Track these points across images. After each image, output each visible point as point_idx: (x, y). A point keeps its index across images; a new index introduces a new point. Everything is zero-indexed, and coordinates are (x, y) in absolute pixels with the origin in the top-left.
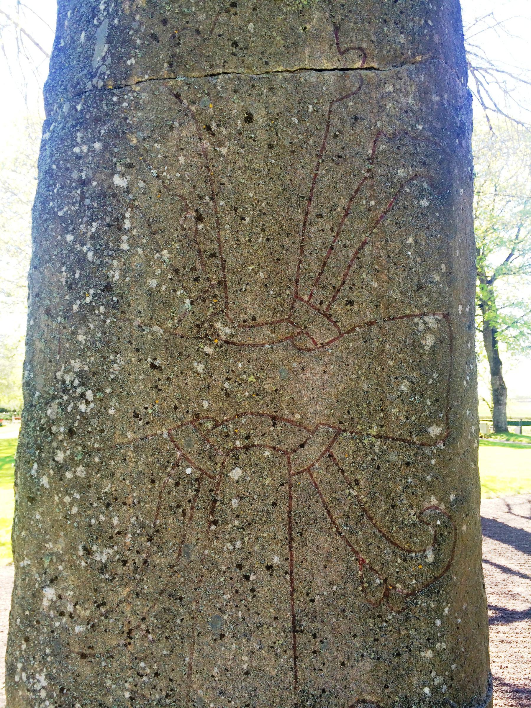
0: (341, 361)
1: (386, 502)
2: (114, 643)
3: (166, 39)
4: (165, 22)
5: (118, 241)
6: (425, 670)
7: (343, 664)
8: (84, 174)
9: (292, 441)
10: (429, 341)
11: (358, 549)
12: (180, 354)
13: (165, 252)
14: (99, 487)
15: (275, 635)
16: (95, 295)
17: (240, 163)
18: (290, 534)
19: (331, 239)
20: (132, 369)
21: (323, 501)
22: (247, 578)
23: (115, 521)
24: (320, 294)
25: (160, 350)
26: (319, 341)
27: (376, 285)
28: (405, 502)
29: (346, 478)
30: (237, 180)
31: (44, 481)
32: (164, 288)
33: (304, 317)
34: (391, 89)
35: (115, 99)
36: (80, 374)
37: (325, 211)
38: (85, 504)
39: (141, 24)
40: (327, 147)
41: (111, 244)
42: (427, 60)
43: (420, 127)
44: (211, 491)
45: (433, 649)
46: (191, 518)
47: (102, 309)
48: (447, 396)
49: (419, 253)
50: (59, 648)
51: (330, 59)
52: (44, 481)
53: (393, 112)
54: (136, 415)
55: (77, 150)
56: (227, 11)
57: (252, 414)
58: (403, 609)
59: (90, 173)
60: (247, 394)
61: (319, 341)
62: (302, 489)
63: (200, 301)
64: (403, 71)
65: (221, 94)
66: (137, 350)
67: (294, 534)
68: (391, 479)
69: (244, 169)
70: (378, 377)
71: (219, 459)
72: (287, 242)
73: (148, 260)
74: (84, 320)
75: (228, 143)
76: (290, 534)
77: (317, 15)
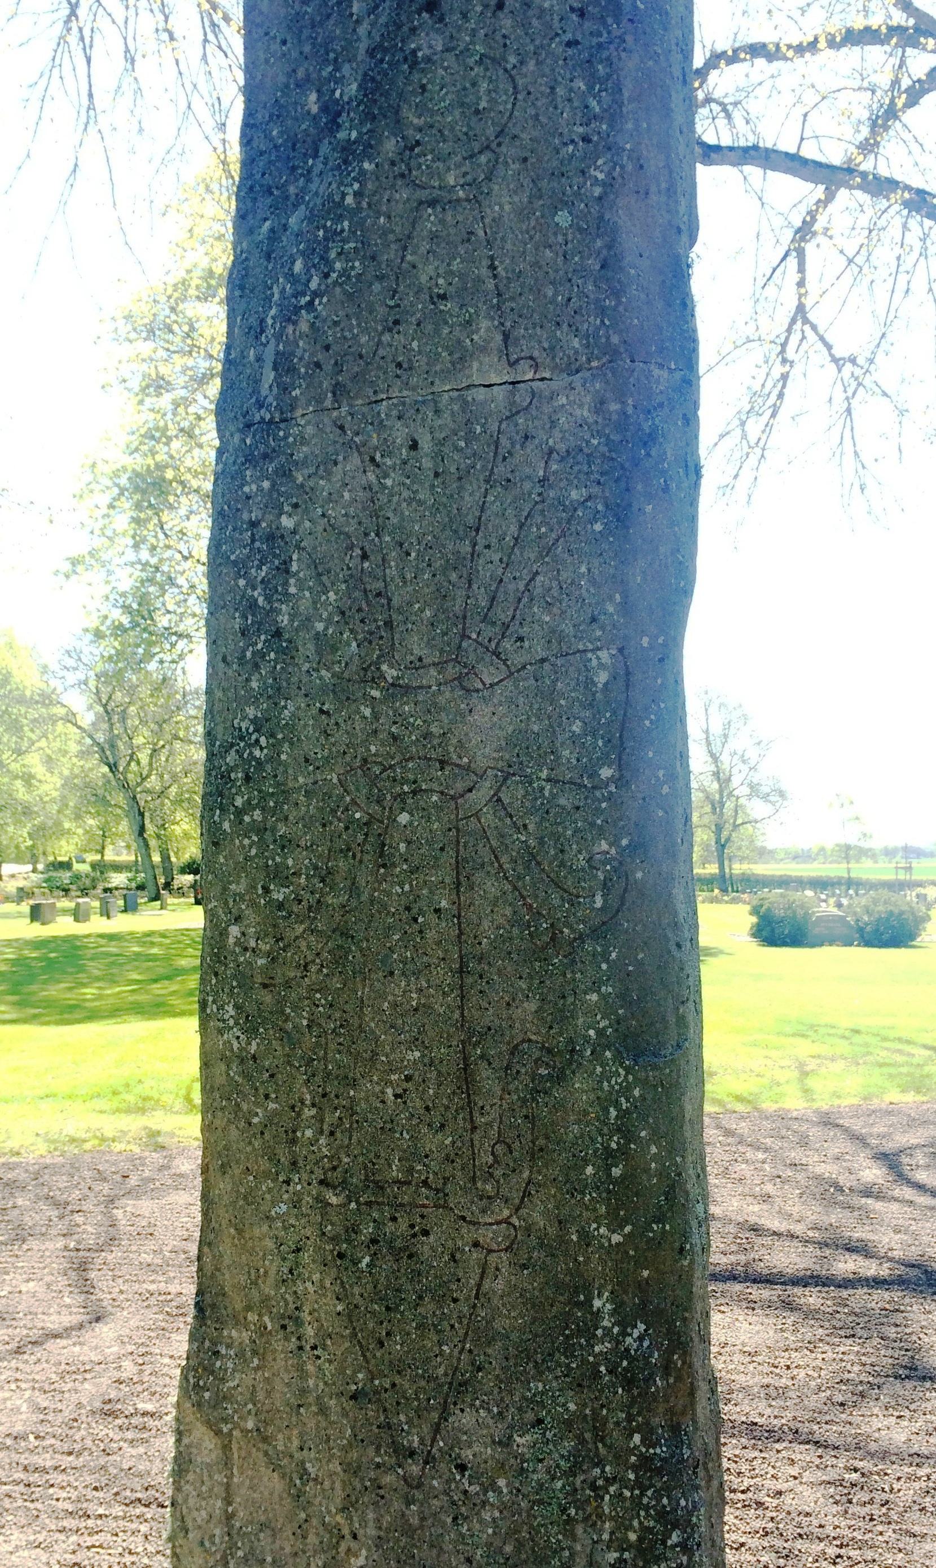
0: (511, 701)
1: (555, 848)
2: (292, 974)
3: (328, 367)
5: (286, 584)
6: (591, 1013)
8: (253, 515)
9: (460, 786)
10: (602, 677)
11: (525, 893)
12: (348, 698)
13: (331, 594)
14: (274, 830)
15: (443, 975)
16: (265, 641)
17: (406, 494)
19: (500, 571)
22: (415, 920)
24: (489, 631)
25: (328, 695)
26: (488, 682)
29: (515, 823)
30: (402, 513)
31: (226, 826)
32: (330, 631)
33: (472, 657)
34: (564, 400)
35: (281, 433)
36: (254, 721)
37: (494, 541)
38: (262, 845)
40: (496, 470)
42: (604, 365)
43: (595, 442)
44: (380, 835)
45: (599, 992)
47: (272, 655)
49: (593, 582)
50: (244, 980)
51: (499, 373)
52: (226, 826)
53: (566, 427)
54: (307, 760)
55: (246, 489)
56: (390, 330)
58: (570, 954)
59: (260, 514)
61: (488, 682)
62: (470, 834)
63: (366, 644)
65: (385, 423)
66: (306, 695)
67: (462, 879)
69: (410, 501)
70: (549, 717)
71: (387, 803)
73: (315, 603)
74: (257, 666)
76: (458, 878)
77: (484, 324)
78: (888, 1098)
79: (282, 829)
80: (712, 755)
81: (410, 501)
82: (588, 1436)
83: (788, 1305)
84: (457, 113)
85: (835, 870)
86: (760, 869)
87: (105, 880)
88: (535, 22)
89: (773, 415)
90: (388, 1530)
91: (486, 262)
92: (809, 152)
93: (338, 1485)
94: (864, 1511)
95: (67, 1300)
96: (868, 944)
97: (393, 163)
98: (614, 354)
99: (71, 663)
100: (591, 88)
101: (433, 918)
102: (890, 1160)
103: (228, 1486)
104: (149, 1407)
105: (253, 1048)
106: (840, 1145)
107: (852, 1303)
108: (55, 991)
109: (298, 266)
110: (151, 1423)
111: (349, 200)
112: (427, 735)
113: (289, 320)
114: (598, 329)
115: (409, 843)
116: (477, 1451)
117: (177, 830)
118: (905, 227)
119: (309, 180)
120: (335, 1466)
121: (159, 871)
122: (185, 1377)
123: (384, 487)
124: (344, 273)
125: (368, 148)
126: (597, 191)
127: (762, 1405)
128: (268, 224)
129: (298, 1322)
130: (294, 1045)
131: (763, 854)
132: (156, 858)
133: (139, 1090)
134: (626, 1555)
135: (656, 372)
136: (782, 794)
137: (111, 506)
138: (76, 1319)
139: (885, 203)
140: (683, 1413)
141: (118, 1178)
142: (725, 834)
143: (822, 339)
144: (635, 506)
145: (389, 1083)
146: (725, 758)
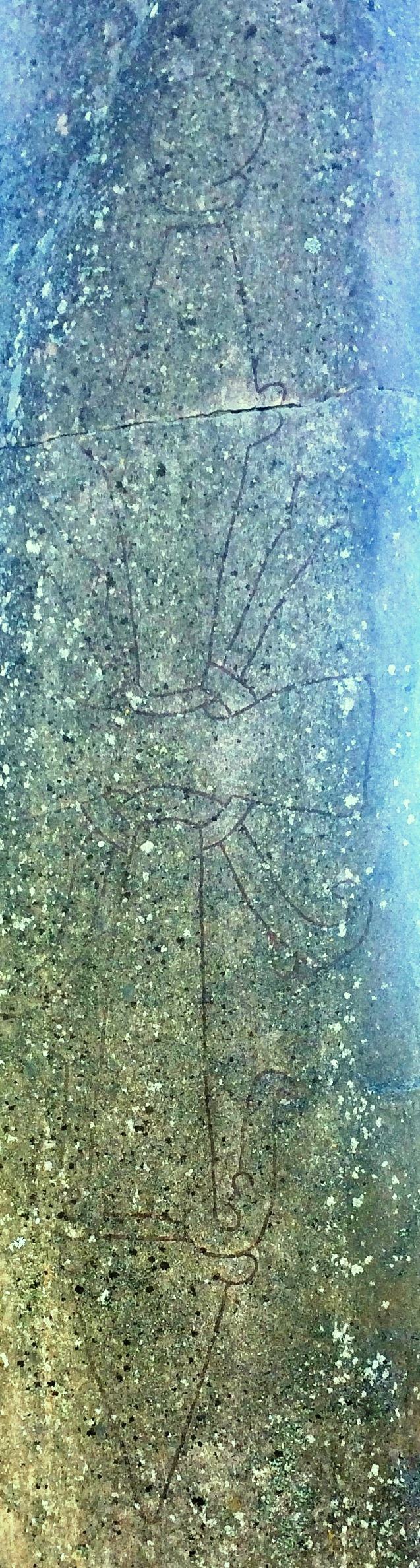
0: (257, 731)
1: (299, 876)
2: (33, 1006)
3: (76, 390)
4: (75, 372)
5: (31, 610)
7: (251, 1034)
9: (204, 814)
10: (348, 705)
14: (16, 859)
15: (184, 1005)
18: (201, 908)
20: (44, 741)
21: (235, 875)
22: (158, 950)
23: (32, 891)
26: (233, 708)
27: (293, 646)
28: (319, 875)
32: (75, 658)
34: (312, 427)
35: (28, 458)
37: (240, 568)
39: (52, 375)
40: (243, 497)
41: (24, 614)
44: (123, 864)
46: (103, 891)
47: (16, 682)
48: (366, 766)
51: (248, 399)
54: (50, 789)
56: (138, 355)
57: (164, 786)
58: (313, 983)
60: (158, 766)
61: (233, 708)
64: (325, 406)
65: (133, 448)
68: (304, 852)
69: (156, 527)
72: (200, 603)
73: (60, 629)
75: (139, 500)
76: (201, 908)
77: (233, 349)
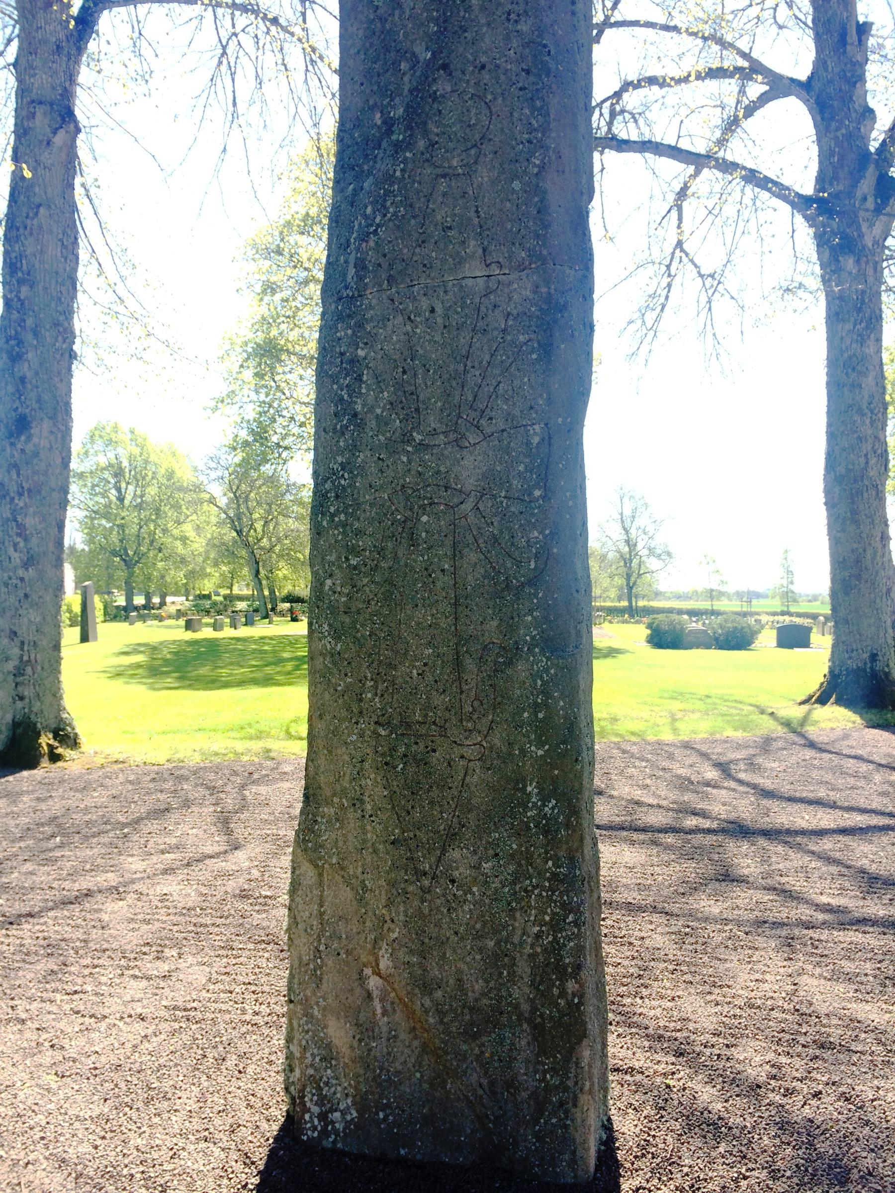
3: (385, 266)
5: (360, 387)
9: (456, 501)
10: (536, 440)
14: (352, 525)
17: (428, 337)
23: (361, 543)
24: (473, 415)
26: (472, 442)
31: (325, 523)
36: (342, 464)
37: (476, 364)
38: (344, 533)
49: (531, 386)
50: (333, 608)
52: (325, 523)
61: (472, 442)
69: (430, 341)
72: (454, 383)
74: (343, 434)
77: (473, 243)
78: (725, 734)
79: (356, 525)
80: (625, 529)
81: (430, 341)
82: (523, 862)
83: (654, 843)
84: (458, 126)
85: (705, 605)
86: (655, 604)
87: (233, 606)
88: (503, 77)
89: (662, 310)
90: (411, 917)
91: (473, 209)
92: (684, 145)
93: (383, 893)
94: (691, 948)
95: (217, 839)
96: (721, 647)
97: (422, 154)
98: (544, 261)
99: (213, 465)
100: (532, 114)
101: (439, 573)
102: (724, 768)
103: (321, 896)
104: (268, 893)
105: (339, 648)
106: (694, 758)
107: (694, 842)
108: (203, 671)
109: (369, 210)
110: (269, 901)
111: (398, 174)
112: (438, 472)
113: (363, 240)
114: (535, 246)
115: (427, 532)
116: (462, 872)
117: (280, 574)
118: (742, 191)
119: (375, 162)
120: (382, 882)
121: (268, 601)
122: (297, 835)
123: (415, 333)
124: (395, 214)
125: (410, 145)
126: (536, 170)
127: (635, 894)
128: (351, 187)
129: (362, 802)
130: (362, 646)
131: (657, 595)
132: (266, 593)
133: (257, 726)
134: (544, 928)
135: (568, 271)
136: (669, 554)
137: (242, 366)
138: (222, 849)
139: (730, 178)
140: (577, 851)
141: (246, 774)
142: (633, 579)
143: (692, 261)
144: (555, 345)
145: (414, 667)
146: (633, 532)
